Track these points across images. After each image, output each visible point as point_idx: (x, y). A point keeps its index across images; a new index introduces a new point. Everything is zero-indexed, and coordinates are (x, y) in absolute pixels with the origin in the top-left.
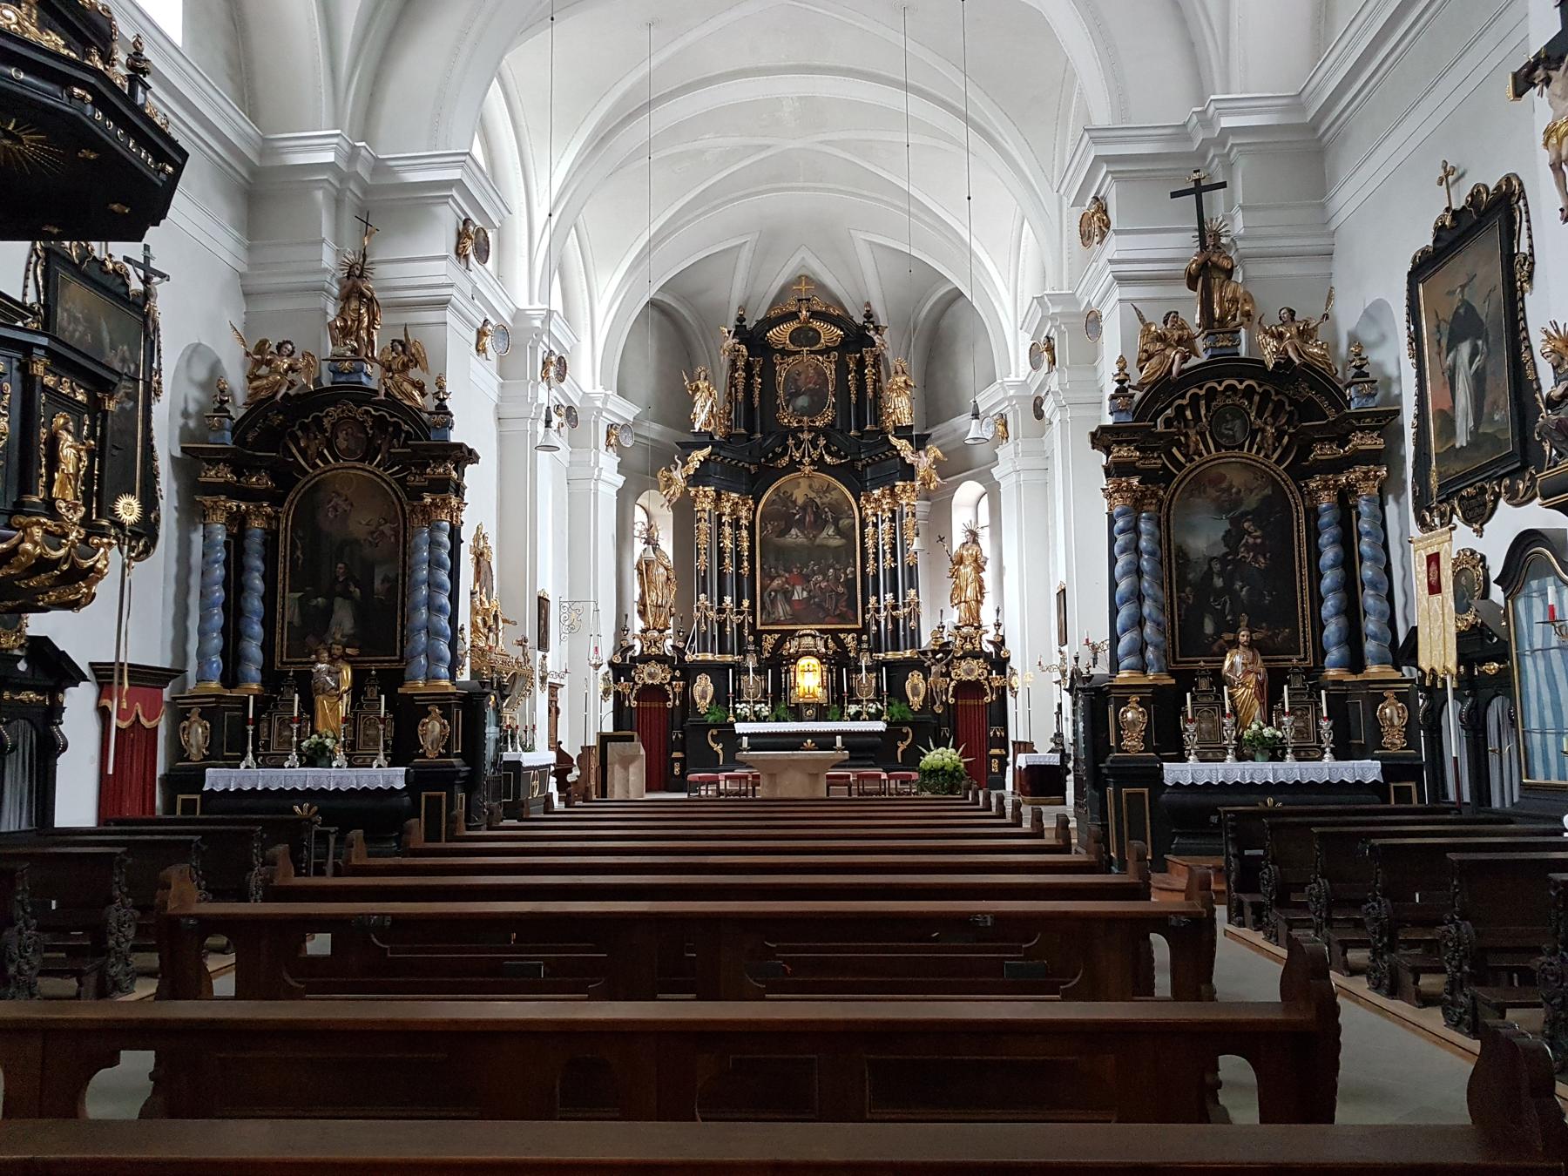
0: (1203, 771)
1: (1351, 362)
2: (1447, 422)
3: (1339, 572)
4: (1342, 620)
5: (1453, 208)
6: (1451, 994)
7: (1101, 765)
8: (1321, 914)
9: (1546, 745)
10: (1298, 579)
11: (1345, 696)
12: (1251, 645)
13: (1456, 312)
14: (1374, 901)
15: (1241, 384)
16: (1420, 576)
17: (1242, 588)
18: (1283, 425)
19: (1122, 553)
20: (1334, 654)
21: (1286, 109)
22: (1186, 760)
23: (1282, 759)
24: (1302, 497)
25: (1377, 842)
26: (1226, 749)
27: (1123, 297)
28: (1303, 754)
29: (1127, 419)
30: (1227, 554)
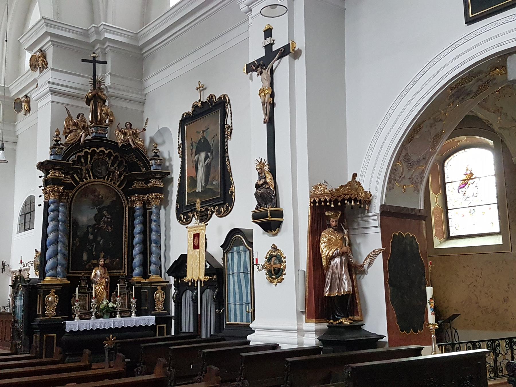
0: (83, 324)
1: (153, 150)
2: (193, 182)
3: (141, 236)
4: (141, 256)
9: (236, 309)
11: (141, 289)
12: (105, 266)
13: (200, 140)
15: (107, 150)
16: (190, 242)
17: (101, 240)
19: (52, 221)
20: (137, 271)
21: (130, 38)
22: (73, 319)
23: (115, 317)
25: (206, 351)
26: (91, 313)
27: (54, 100)
30: (95, 225)
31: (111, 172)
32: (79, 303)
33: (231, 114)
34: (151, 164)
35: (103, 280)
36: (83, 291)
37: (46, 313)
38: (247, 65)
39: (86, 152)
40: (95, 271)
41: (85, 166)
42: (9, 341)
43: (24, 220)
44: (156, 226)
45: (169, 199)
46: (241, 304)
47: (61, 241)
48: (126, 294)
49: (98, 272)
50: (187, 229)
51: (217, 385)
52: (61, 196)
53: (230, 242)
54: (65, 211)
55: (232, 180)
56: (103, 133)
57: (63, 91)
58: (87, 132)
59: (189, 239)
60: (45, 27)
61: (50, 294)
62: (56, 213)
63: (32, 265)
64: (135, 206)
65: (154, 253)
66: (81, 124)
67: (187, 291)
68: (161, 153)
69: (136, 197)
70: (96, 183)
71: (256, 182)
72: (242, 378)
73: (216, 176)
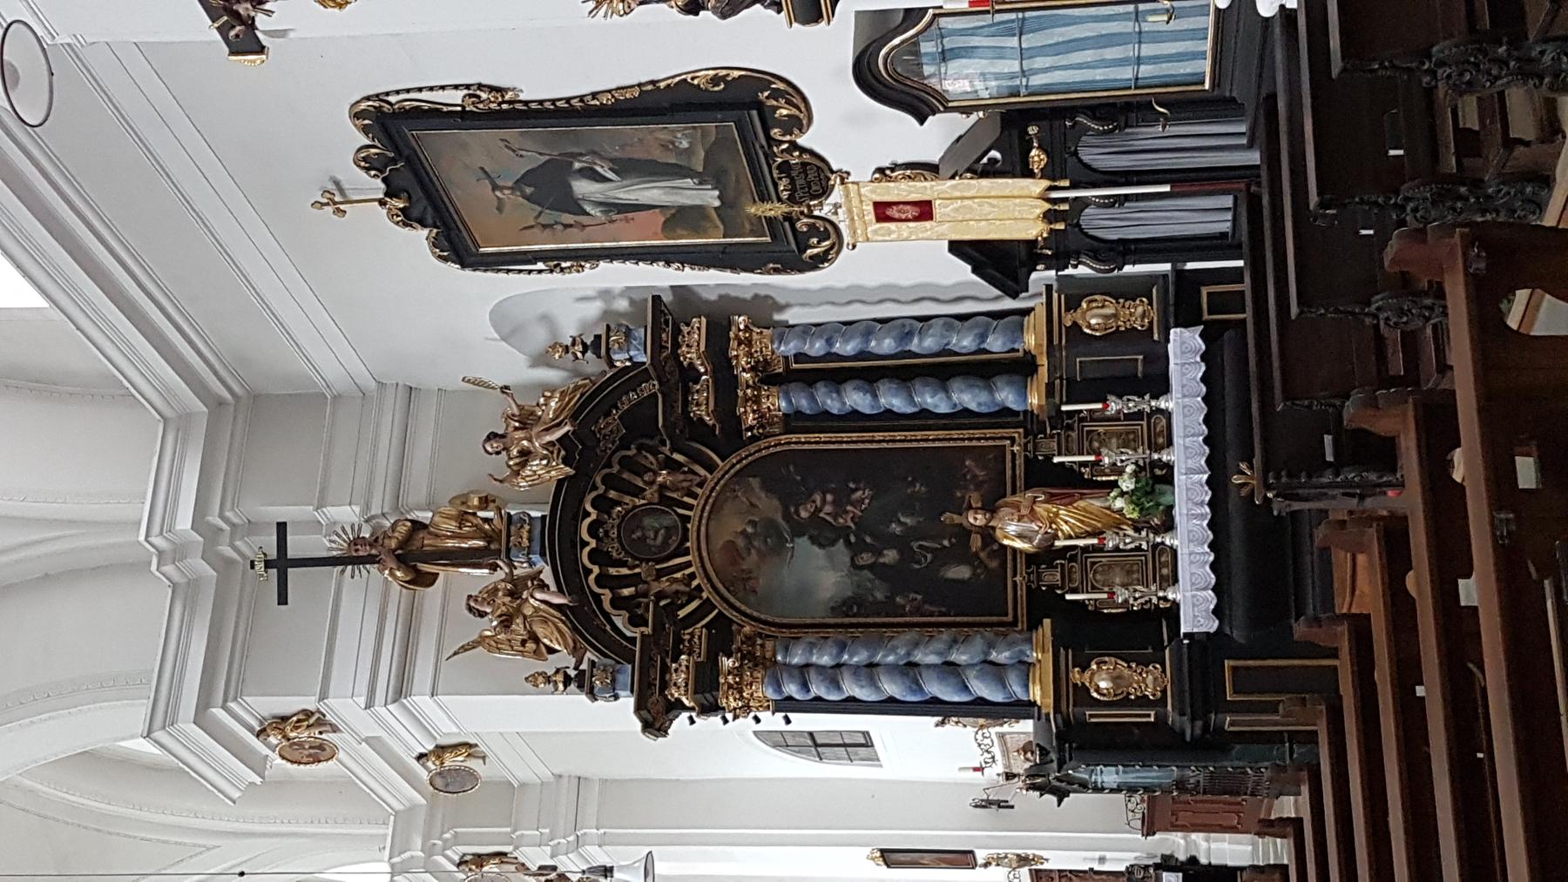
0: (1192, 574)
1: (577, 358)
2: (681, 218)
4: (956, 384)
5: (381, 196)
6: (1542, 78)
7: (1188, 738)
8: (1427, 308)
10: (891, 445)
11: (1071, 381)
12: (991, 508)
14: (1403, 208)
15: (588, 514)
18: (657, 459)
19: (839, 688)
20: (1006, 396)
21: (183, 441)
22: (1175, 605)
23: (1169, 467)
24: (766, 437)
25: (1314, 199)
26: (1155, 546)
28: (1161, 440)
29: (626, 673)
30: (848, 543)
31: (662, 496)
32: (1118, 590)
33: (420, 90)
34: (628, 364)
35: (1040, 509)
36: (1077, 576)
37: (1154, 695)
38: (232, 53)
39: (598, 581)
40: (1006, 537)
41: (646, 582)
42: (1239, 817)
43: (836, 749)
44: (852, 338)
45: (748, 296)
46: (1140, 37)
47: (909, 654)
48: (1089, 432)
49: (1013, 528)
50: (858, 244)
51: (1457, 236)
52: (755, 661)
53: (906, 89)
54: (803, 646)
55: (669, 81)
56: (527, 527)
57: (396, 648)
58: (529, 583)
59: (894, 236)
60: (181, 725)
61: (1088, 684)
62: (813, 675)
63: (987, 735)
64: (780, 410)
65: (945, 341)
66: (504, 604)
67: (1081, 222)
68: (585, 325)
69: (746, 412)
70: (703, 546)
71: (675, 10)
72: (1426, 67)
73: (657, 139)
